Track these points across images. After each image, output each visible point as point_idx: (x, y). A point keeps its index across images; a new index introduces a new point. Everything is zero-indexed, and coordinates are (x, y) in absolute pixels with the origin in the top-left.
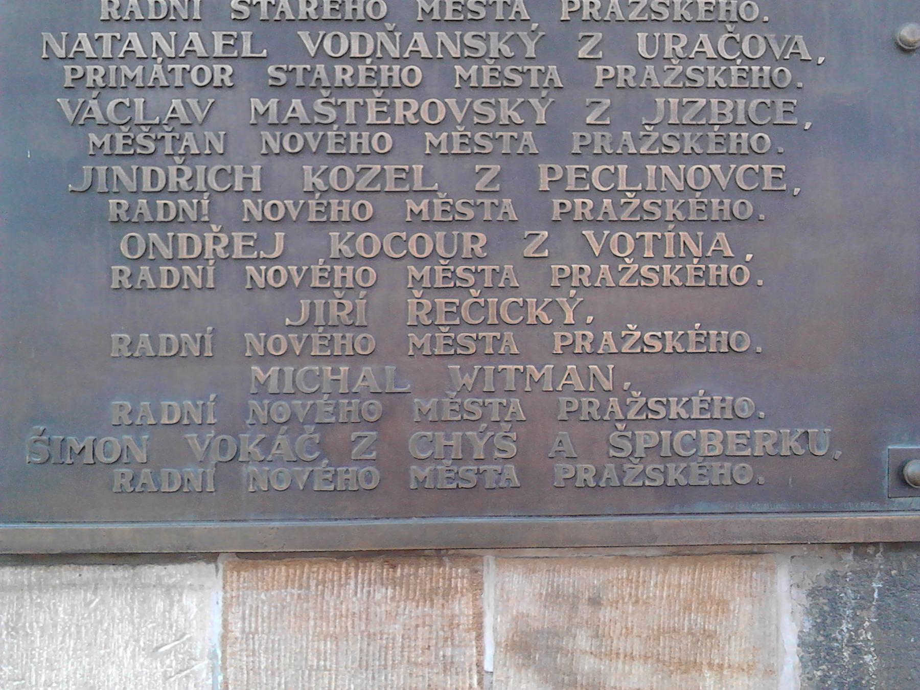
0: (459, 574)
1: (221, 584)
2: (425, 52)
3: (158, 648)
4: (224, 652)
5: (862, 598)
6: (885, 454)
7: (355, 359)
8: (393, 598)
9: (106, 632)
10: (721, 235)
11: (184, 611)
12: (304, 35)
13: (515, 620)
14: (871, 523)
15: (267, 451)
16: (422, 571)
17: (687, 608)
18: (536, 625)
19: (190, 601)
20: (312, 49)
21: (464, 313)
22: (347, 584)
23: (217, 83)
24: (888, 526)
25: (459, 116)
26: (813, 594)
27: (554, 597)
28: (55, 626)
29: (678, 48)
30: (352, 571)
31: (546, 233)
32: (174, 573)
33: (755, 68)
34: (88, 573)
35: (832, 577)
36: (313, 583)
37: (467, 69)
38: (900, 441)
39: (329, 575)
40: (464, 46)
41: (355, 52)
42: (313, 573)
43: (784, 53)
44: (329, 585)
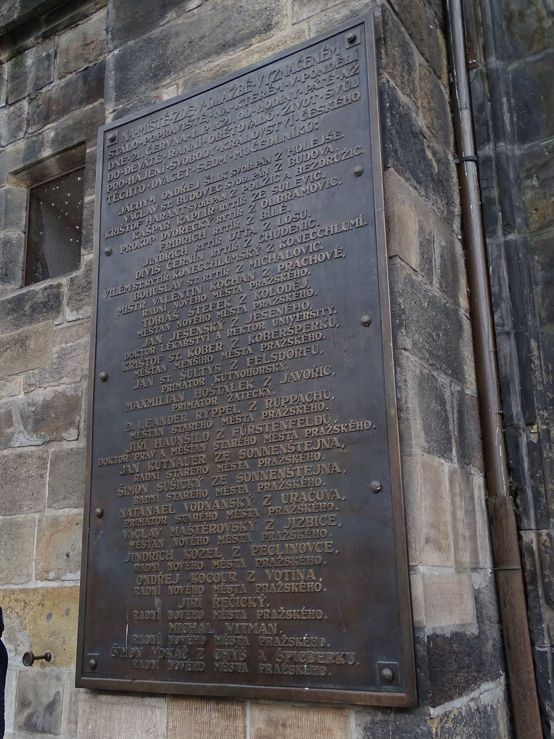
0: (238, 709)
1: (166, 707)
2: (218, 507)
3: (148, 730)
4: (167, 734)
5: (385, 734)
6: (377, 665)
7: (198, 621)
8: (218, 717)
9: (134, 722)
10: (311, 570)
11: (156, 716)
12: (185, 504)
13: (257, 730)
14: (371, 696)
15: (173, 654)
16: (227, 707)
17: (317, 731)
18: (264, 733)
19: (158, 712)
20: (187, 509)
21: (230, 603)
22: (204, 710)
23: (162, 523)
24: (379, 698)
25: (228, 530)
26: (365, 729)
27: (270, 722)
28: (121, 719)
29: (294, 499)
30: (205, 704)
31: (254, 572)
32: (153, 701)
33: (321, 504)
34: (131, 699)
35: (372, 723)
36: (193, 709)
37: (230, 511)
38: (383, 660)
39: (198, 706)
40: (286, 473)
41: (199, 510)
42: (194, 705)
43: (330, 497)
44: (198, 710)
